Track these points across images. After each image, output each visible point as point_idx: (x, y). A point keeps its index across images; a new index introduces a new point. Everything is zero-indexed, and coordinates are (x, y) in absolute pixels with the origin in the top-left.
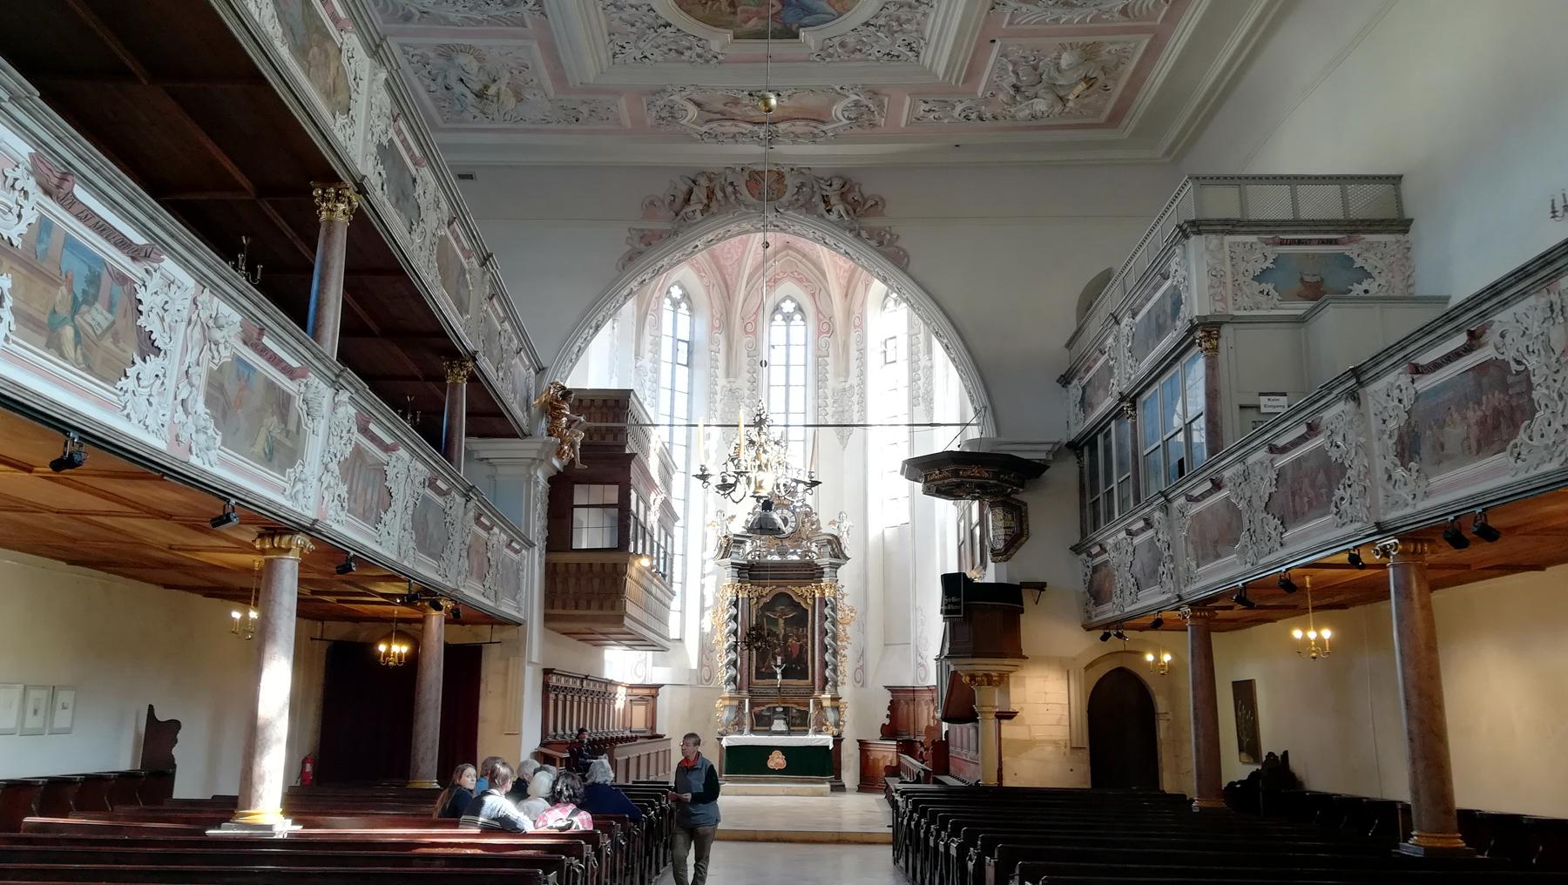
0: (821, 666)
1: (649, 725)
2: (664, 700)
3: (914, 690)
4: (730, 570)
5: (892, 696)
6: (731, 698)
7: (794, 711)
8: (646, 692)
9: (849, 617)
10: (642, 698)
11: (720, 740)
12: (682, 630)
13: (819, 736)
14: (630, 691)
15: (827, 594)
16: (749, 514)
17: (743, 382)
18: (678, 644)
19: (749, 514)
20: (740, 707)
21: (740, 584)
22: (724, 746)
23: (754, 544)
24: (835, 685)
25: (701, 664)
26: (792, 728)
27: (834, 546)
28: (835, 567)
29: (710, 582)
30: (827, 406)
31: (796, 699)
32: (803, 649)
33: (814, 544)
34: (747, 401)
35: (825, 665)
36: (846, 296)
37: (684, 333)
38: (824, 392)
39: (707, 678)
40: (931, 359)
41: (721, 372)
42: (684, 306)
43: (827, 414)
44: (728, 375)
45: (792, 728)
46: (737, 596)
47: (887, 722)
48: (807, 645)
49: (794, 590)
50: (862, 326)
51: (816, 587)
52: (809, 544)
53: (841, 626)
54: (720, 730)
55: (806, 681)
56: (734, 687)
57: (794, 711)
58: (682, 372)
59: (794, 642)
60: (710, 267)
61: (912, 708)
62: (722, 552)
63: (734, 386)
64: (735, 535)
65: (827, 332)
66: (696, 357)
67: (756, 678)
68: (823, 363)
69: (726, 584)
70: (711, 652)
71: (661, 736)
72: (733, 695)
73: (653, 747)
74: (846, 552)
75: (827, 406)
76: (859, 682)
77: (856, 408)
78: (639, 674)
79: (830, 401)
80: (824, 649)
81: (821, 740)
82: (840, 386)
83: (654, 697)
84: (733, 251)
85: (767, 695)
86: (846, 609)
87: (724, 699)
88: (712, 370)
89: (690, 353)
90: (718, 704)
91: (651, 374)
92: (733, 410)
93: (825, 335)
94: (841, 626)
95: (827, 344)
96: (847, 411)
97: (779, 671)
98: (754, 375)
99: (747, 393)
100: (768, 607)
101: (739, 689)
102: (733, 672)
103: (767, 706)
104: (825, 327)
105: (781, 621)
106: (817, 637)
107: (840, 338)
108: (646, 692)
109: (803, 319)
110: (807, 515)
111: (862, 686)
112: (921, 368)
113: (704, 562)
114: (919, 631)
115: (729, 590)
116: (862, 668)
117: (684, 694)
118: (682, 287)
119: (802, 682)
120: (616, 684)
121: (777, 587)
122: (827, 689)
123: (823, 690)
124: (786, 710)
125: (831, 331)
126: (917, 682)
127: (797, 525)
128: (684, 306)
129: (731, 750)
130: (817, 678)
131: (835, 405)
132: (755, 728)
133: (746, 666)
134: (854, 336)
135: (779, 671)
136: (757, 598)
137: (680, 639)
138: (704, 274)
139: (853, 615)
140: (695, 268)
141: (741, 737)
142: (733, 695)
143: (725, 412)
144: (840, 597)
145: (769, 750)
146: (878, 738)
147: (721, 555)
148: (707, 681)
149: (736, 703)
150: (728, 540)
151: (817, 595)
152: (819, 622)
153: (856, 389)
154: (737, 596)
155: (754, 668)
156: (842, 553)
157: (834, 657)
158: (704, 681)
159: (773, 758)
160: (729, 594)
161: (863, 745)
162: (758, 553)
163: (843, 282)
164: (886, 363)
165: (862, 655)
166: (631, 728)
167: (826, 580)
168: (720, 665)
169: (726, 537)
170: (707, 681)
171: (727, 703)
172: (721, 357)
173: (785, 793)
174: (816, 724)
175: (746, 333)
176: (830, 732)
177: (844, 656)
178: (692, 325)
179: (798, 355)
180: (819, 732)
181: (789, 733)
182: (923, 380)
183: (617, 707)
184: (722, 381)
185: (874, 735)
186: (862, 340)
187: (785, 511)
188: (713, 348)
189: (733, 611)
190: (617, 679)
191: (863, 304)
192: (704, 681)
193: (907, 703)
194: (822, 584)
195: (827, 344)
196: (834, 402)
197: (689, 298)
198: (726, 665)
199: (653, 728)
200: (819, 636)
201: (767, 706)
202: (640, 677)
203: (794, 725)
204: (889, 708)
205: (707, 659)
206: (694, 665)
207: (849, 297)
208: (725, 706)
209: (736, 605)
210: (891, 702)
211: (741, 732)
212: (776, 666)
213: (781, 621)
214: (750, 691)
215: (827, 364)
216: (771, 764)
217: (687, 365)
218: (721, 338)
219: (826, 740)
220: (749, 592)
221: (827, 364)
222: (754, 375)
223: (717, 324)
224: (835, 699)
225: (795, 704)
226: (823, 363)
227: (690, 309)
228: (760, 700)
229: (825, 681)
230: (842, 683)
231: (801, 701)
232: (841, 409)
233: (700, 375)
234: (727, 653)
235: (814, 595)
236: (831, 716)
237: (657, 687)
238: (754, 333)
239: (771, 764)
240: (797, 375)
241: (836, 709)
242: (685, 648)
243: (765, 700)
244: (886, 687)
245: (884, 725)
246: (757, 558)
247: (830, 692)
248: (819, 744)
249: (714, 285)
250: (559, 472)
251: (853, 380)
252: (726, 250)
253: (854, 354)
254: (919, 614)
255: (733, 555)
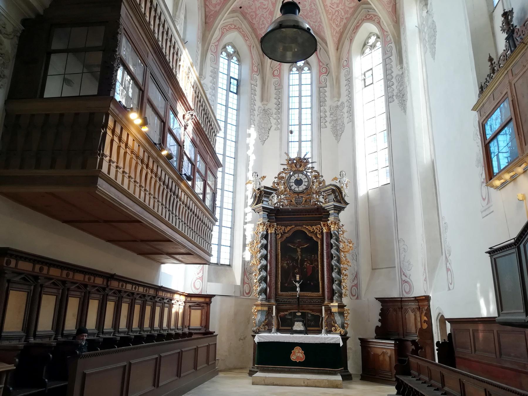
0: (329, 282)
1: (204, 324)
2: (215, 306)
3: (401, 301)
4: (262, 213)
5: (382, 305)
6: (262, 305)
7: (309, 315)
8: (201, 300)
9: (348, 247)
10: (199, 305)
11: (254, 336)
12: (231, 259)
13: (330, 336)
14: (189, 299)
15: (332, 229)
16: (275, 178)
17: (272, 105)
18: (228, 268)
19: (275, 178)
20: (269, 312)
21: (269, 223)
22: (256, 342)
23: (279, 197)
24: (341, 296)
25: (243, 282)
26: (308, 328)
27: (337, 194)
28: (338, 209)
29: (250, 230)
30: (326, 117)
31: (311, 307)
32: (315, 270)
33: (321, 197)
34: (275, 116)
35: (332, 281)
36: (337, 49)
37: (234, 73)
38: (324, 108)
39: (247, 292)
40: (402, 68)
41: (258, 98)
42: (235, 58)
43: (326, 122)
44: (262, 100)
45: (308, 328)
46: (267, 232)
47: (379, 324)
48: (318, 267)
49: (308, 229)
50: (349, 65)
51: (324, 225)
52: (317, 197)
53: (342, 253)
54: (255, 329)
55: (318, 293)
56: (264, 296)
57: (309, 315)
58: (233, 98)
59: (308, 265)
60: (251, 35)
61: (400, 314)
62: (256, 201)
63: (266, 108)
64: (265, 187)
65: (326, 73)
66: (242, 89)
67: (281, 291)
68: (323, 91)
69: (259, 223)
70: (250, 274)
71: (212, 333)
72: (264, 302)
73: (205, 342)
74: (346, 199)
75: (326, 117)
76: (355, 296)
77: (346, 115)
78: (197, 287)
79: (328, 114)
80: (331, 269)
81: (333, 338)
82: (335, 105)
83: (208, 304)
84: (265, 22)
85: (290, 303)
86: (346, 241)
87: (257, 305)
88: (252, 95)
89: (238, 86)
90: (254, 309)
91: (211, 90)
92: (266, 122)
93: (325, 75)
94: (342, 253)
95: (326, 80)
96: (340, 119)
97: (298, 285)
98: (279, 120)
99: (274, 111)
100: (290, 240)
101: (268, 299)
102: (264, 285)
103: (289, 312)
104: (324, 70)
105: (299, 250)
106: (325, 260)
107: (334, 75)
108: (201, 300)
109: (309, 69)
110: (316, 177)
111: (357, 298)
112: (394, 77)
113: (245, 214)
114: (402, 256)
115: (261, 227)
116: (356, 285)
117: (231, 302)
118: (233, 47)
119: (315, 294)
120: (173, 292)
121: (296, 226)
122: (334, 299)
123: (332, 300)
124: (304, 315)
125: (328, 72)
126: (403, 294)
127: (309, 184)
128: (235, 58)
129: (262, 345)
130: (326, 290)
131: (332, 116)
132: (281, 328)
133: (273, 281)
134: (343, 72)
135: (298, 285)
136: (281, 234)
137: (229, 265)
138: (247, 39)
139: (351, 245)
140: (242, 34)
141: (269, 334)
142: (264, 302)
143: (260, 122)
144: (341, 233)
145: (292, 346)
146: (374, 337)
147: (256, 202)
148: (247, 294)
149: (266, 309)
150: (261, 192)
151: (325, 231)
152: (327, 250)
153: (346, 104)
154: (267, 232)
155: (279, 283)
156: (343, 199)
157: (339, 275)
158: (245, 293)
159: (294, 352)
160: (261, 230)
161: (364, 343)
162: (282, 203)
163: (336, 40)
164: (365, 86)
165: (356, 276)
166: (189, 326)
167: (331, 218)
168: (255, 281)
169: (259, 189)
170: (247, 294)
171: (260, 308)
172: (258, 89)
173: (306, 383)
174: (327, 326)
175: (274, 75)
176: (339, 332)
177: (345, 275)
178: (240, 70)
179: (306, 90)
180: (329, 332)
181: (306, 332)
182: (396, 84)
183: (174, 310)
184: (258, 103)
185: (370, 334)
186: (350, 73)
187: (301, 175)
188: (253, 82)
189: (264, 241)
190: (172, 286)
191: (349, 52)
192: (245, 293)
193: (395, 310)
194: (329, 222)
195: (326, 80)
196: (331, 115)
197: (238, 53)
198: (259, 281)
199: (207, 326)
200: (327, 259)
201: (289, 312)
202: (198, 289)
203: (310, 326)
204: (380, 314)
205: (248, 279)
206: (238, 282)
207: (339, 50)
208: (258, 311)
209: (266, 237)
210: (382, 310)
211: (270, 331)
212: (296, 281)
213: (299, 250)
214: (276, 301)
215: (326, 92)
216: (293, 358)
217: (237, 93)
218: (258, 78)
219: (335, 338)
220: (276, 229)
221: (326, 92)
222: (279, 100)
223: (255, 69)
224: (341, 306)
225: (310, 310)
226: (323, 91)
227: (238, 60)
228: (284, 307)
229: (332, 293)
230: (345, 295)
231: (315, 308)
232: (335, 118)
233: (245, 98)
234: (260, 272)
235: (322, 231)
236: (338, 319)
237: (211, 297)
238: (279, 76)
239: (293, 358)
240: (307, 102)
241: (341, 314)
242: (232, 269)
243: (288, 307)
244: (377, 299)
245: (377, 327)
246: (281, 207)
247: (337, 301)
248: (332, 342)
249: (253, 47)
250: (38, 15)
251: (344, 98)
252: (261, 23)
253: (343, 82)
254: (401, 244)
255: (264, 203)
